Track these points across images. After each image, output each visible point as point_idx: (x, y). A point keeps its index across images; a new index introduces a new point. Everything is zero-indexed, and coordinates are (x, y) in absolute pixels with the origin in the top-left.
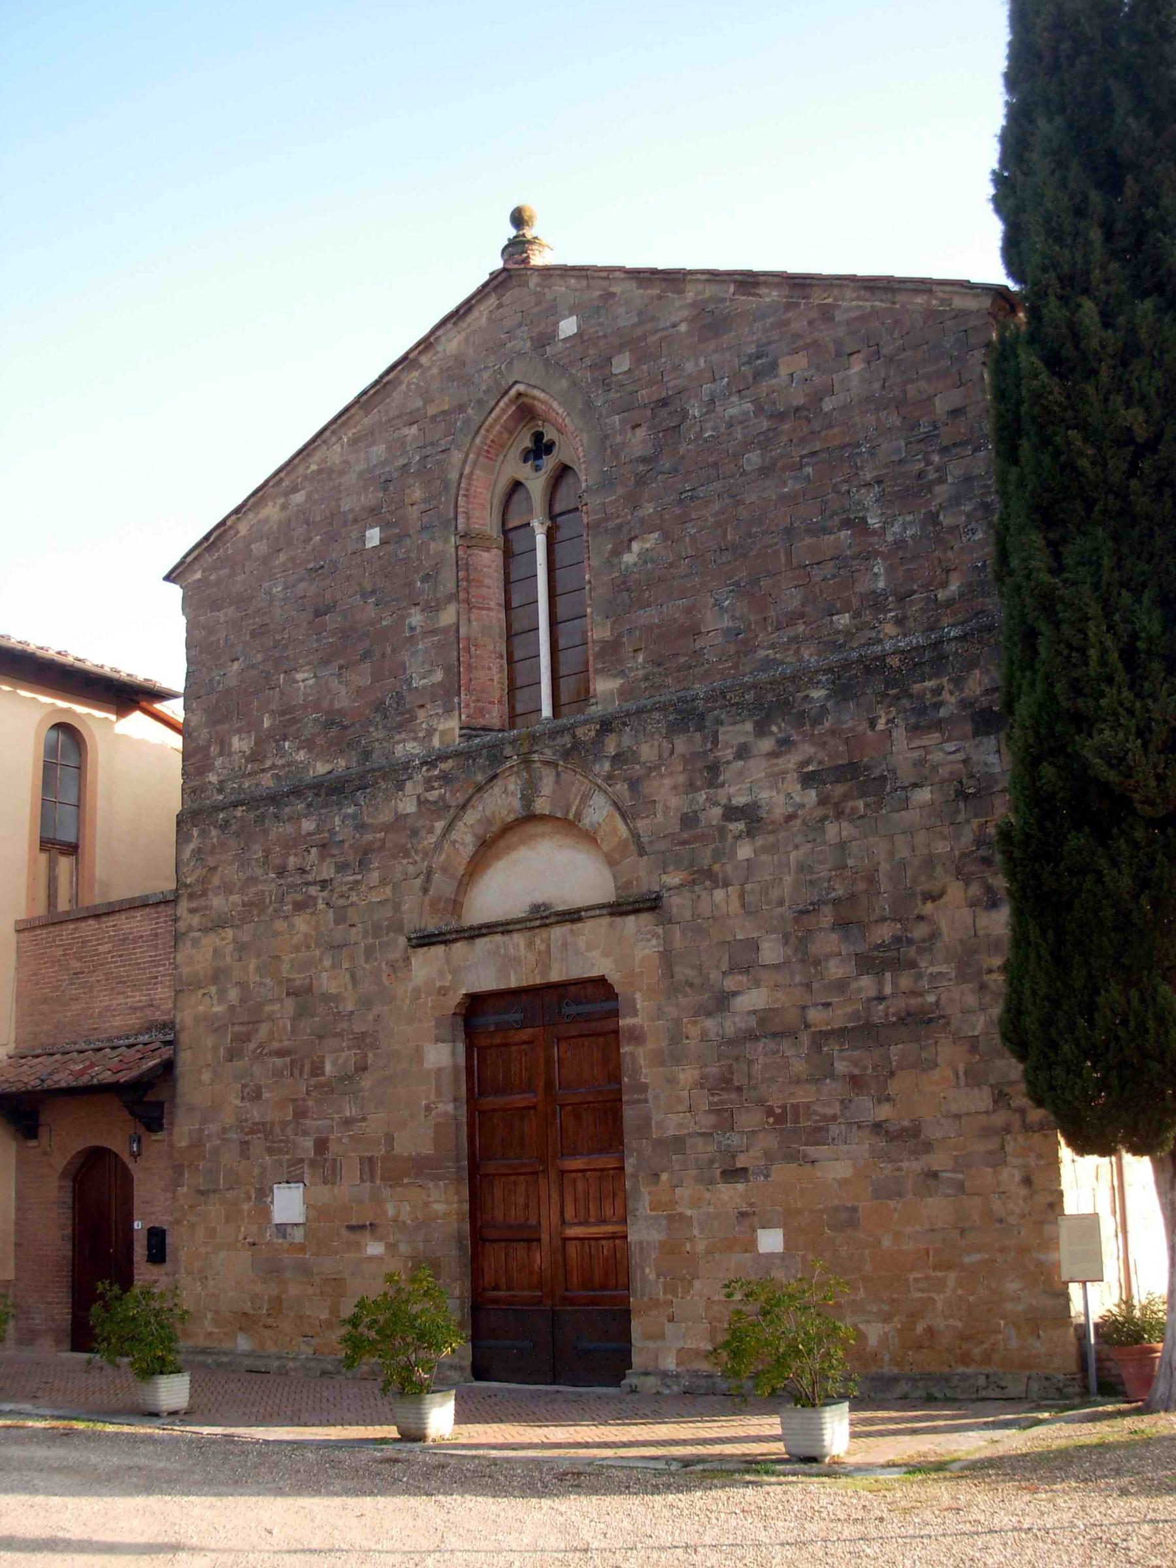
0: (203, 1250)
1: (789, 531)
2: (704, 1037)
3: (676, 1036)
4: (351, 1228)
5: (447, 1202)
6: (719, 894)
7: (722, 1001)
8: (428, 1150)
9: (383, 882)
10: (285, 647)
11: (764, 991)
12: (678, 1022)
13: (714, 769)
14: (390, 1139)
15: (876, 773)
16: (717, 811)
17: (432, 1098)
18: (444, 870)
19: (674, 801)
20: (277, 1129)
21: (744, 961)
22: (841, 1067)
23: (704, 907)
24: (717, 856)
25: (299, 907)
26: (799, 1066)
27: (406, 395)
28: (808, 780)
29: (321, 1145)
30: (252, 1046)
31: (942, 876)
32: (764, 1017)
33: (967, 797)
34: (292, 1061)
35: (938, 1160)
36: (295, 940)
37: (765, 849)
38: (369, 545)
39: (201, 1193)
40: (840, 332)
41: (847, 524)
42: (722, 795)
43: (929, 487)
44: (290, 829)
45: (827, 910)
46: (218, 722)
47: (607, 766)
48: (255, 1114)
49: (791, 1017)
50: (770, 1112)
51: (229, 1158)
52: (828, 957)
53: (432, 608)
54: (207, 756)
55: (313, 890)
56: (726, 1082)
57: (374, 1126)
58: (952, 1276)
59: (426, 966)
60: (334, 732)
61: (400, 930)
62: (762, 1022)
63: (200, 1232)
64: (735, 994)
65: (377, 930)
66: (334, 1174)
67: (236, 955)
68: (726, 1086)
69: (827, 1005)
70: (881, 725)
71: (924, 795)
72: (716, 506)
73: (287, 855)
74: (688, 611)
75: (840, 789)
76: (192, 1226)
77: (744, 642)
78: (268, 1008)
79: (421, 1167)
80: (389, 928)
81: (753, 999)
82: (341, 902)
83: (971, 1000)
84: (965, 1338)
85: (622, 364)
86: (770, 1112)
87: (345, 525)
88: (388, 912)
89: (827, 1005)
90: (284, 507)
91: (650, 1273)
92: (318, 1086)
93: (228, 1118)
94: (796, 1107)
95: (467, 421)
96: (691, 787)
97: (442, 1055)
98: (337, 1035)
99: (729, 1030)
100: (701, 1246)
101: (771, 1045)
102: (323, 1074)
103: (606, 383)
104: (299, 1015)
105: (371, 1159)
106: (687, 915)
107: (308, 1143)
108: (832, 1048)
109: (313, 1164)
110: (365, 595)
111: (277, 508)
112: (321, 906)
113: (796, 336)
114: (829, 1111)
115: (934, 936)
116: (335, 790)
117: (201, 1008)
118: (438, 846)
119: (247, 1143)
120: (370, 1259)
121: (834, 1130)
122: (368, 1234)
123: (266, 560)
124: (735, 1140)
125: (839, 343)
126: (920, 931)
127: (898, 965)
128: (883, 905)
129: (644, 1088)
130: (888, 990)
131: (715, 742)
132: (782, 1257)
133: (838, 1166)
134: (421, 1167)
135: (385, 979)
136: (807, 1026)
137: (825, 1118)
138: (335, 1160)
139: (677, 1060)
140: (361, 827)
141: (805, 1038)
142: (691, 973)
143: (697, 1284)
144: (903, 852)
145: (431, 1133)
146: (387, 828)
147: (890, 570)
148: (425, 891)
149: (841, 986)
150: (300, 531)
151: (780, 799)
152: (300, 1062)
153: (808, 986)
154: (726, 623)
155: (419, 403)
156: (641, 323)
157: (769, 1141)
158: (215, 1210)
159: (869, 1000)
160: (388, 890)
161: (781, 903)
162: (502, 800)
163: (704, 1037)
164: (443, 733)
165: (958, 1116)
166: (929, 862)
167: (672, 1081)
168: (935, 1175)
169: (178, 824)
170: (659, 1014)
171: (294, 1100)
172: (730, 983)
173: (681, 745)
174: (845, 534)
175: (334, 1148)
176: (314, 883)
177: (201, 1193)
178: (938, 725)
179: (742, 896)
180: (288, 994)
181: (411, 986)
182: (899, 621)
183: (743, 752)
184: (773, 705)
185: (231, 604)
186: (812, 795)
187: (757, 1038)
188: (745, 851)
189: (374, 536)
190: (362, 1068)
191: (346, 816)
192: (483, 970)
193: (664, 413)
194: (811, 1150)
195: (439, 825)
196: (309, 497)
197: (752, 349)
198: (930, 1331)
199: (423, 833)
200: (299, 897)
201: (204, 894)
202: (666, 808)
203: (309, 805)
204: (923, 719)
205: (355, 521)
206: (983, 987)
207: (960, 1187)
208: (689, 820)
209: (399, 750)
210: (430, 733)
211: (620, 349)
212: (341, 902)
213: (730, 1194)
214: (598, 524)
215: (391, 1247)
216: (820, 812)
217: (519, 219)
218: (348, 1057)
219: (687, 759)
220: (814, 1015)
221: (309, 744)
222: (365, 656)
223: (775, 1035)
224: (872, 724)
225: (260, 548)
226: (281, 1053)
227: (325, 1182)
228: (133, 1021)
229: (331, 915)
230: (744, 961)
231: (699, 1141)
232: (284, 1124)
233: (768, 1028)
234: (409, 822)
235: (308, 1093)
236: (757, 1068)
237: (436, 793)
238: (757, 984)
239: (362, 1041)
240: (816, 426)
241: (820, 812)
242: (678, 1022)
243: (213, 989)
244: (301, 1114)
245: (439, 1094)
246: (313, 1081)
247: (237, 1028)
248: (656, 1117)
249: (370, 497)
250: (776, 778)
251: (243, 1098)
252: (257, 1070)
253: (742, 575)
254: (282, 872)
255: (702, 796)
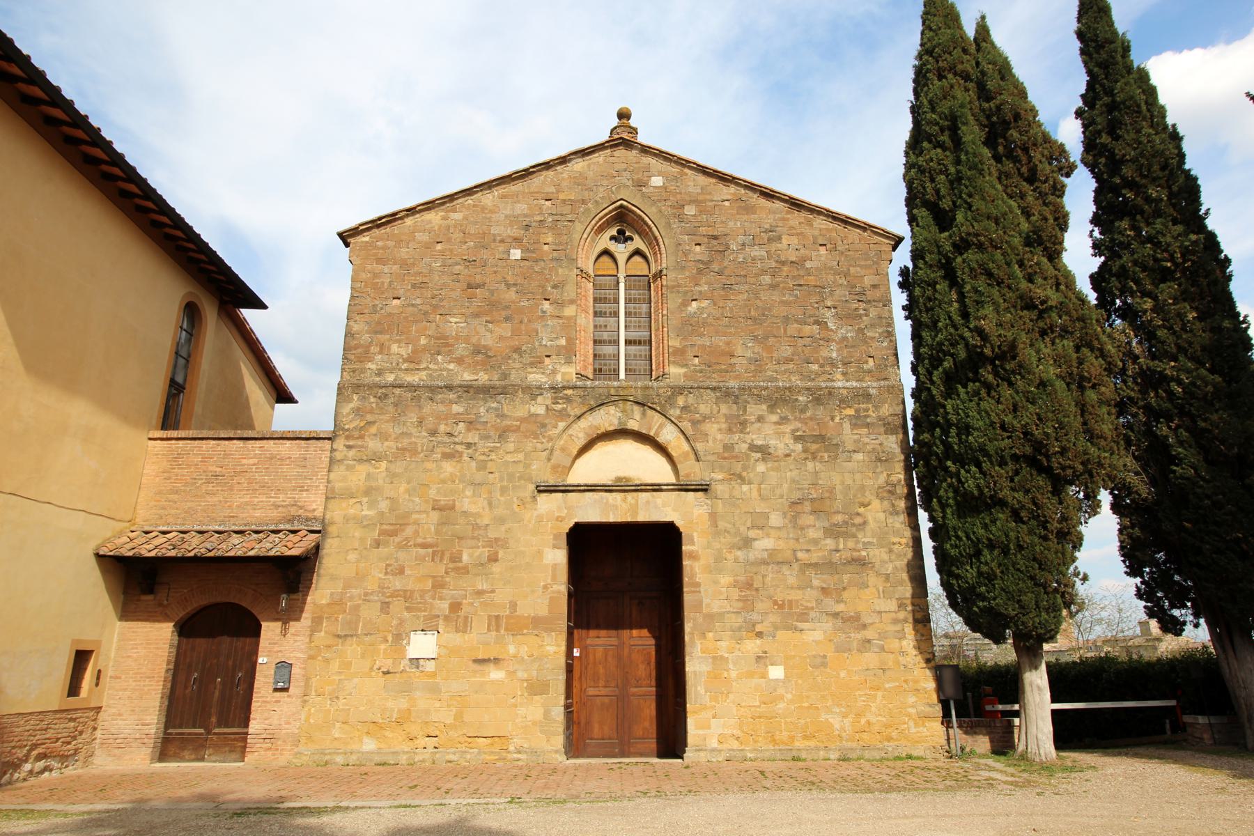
0: (337, 678)
1: (786, 318)
2: (736, 560)
3: (719, 559)
4: (476, 661)
5: (558, 645)
6: (745, 488)
7: (747, 543)
8: (544, 612)
9: (517, 451)
10: (441, 300)
11: (772, 540)
12: (720, 551)
13: (744, 424)
14: (513, 606)
15: (834, 442)
16: (745, 446)
17: (549, 581)
18: (563, 449)
19: (719, 437)
20: (417, 595)
21: (760, 523)
22: (816, 583)
23: (736, 493)
24: (745, 468)
25: (447, 456)
26: (792, 580)
27: (543, 183)
28: (797, 439)
29: (455, 607)
30: (397, 539)
31: (869, 496)
32: (772, 553)
33: (880, 460)
34: (434, 552)
35: (869, 634)
36: (442, 476)
37: (772, 469)
38: (512, 258)
39: (339, 636)
40: (816, 233)
41: (817, 323)
42: (748, 438)
43: (861, 316)
44: (441, 408)
45: (807, 503)
46: (376, 333)
47: (678, 412)
48: (397, 583)
49: (788, 554)
50: (775, 603)
51: (370, 612)
52: (809, 526)
53: (560, 304)
54: (367, 351)
55: (459, 448)
56: (749, 585)
57: (503, 595)
58: (880, 694)
59: (548, 503)
60: (480, 357)
61: (530, 479)
62: (770, 555)
63: (335, 665)
64: (755, 539)
65: (511, 477)
66: (465, 626)
67: (388, 480)
68: (748, 588)
69: (808, 551)
70: (837, 420)
71: (860, 456)
72: (745, 296)
73: (439, 424)
74: (728, 344)
75: (814, 447)
76: (327, 661)
77: (760, 366)
78: (415, 516)
79: (538, 624)
80: (520, 478)
81: (765, 544)
82: (483, 458)
83: (886, 557)
84: (888, 726)
85: (690, 210)
86: (775, 603)
87: (494, 241)
88: (520, 468)
89: (808, 551)
90: (444, 218)
91: (701, 690)
92: (457, 569)
93: (371, 585)
94: (790, 601)
95: (588, 210)
96: (730, 430)
97: (558, 557)
98: (473, 538)
99: (752, 557)
100: (734, 674)
101: (776, 568)
102: (461, 561)
103: (680, 218)
104: (441, 523)
105: (497, 617)
106: (727, 496)
107: (444, 606)
108: (811, 573)
109: (446, 618)
110: (508, 286)
111: (439, 217)
112: (465, 458)
113: (792, 228)
114: (809, 605)
115: (865, 523)
116: (486, 391)
117: (352, 511)
118: (560, 436)
119: (388, 603)
120: (493, 682)
121: (812, 614)
122: (492, 665)
123: (427, 246)
124: (755, 617)
125: (815, 238)
126: (858, 520)
127: (846, 535)
128: (838, 505)
129: (698, 585)
130: (841, 547)
131: (745, 410)
132: (784, 681)
133: (816, 634)
134: (538, 624)
135: (515, 506)
136: (797, 560)
137: (807, 608)
138: (466, 618)
139: (720, 571)
140: (503, 416)
141: (796, 566)
142: (729, 526)
143: (731, 696)
144: (849, 482)
145: (547, 602)
146: (522, 420)
147: (838, 350)
148: (549, 460)
149: (815, 542)
150: (457, 236)
151: (781, 446)
152: (442, 551)
153: (797, 540)
154: (749, 354)
155: (553, 189)
156: (702, 193)
157: (773, 618)
158: (352, 649)
159: (832, 551)
160: (521, 457)
161: (782, 497)
162: (608, 418)
163: (736, 560)
164: (564, 374)
165: (880, 612)
166: (862, 488)
167: (716, 582)
168: (869, 641)
169: (339, 389)
170: (709, 546)
171: (434, 577)
172: (752, 534)
173: (724, 409)
174: (815, 327)
175: (465, 609)
176: (462, 443)
177: (339, 636)
178: (867, 425)
179: (759, 490)
180: (434, 509)
181: (535, 513)
182: (844, 374)
183: (760, 419)
184: (779, 399)
185: (395, 264)
186: (799, 447)
187: (768, 564)
188: (761, 467)
189: (516, 254)
190: (493, 559)
191: (490, 408)
192: (594, 510)
193: (714, 242)
194: (800, 625)
195: (562, 425)
196: (465, 218)
197: (767, 226)
198: (869, 723)
199: (549, 427)
200: (447, 450)
201: (361, 437)
202: (715, 439)
203: (460, 397)
204: (858, 421)
205: (502, 241)
206: (891, 551)
207: (882, 649)
208: (728, 447)
209: (531, 377)
210: (554, 372)
211: (690, 203)
212: (483, 458)
213: (753, 646)
214: (673, 287)
215: (512, 674)
216: (804, 456)
217: (624, 115)
218: (483, 552)
219: (727, 417)
220: (800, 555)
221: (460, 361)
222: (507, 319)
223: (778, 563)
224: (832, 419)
225: (423, 237)
226: (424, 546)
227: (457, 631)
228: (275, 514)
229: (474, 464)
230: (760, 523)
231: (733, 616)
232: (423, 593)
233: (773, 559)
234: (539, 419)
235: (446, 573)
236: (768, 579)
237: (560, 406)
238: (768, 536)
239: (494, 542)
240: (802, 273)
241: (804, 456)
242: (720, 551)
243: (365, 500)
244: (439, 585)
245: (554, 578)
246: (451, 565)
247: (384, 527)
248: (705, 601)
249: (515, 232)
250: (780, 435)
251: (386, 573)
252: (402, 555)
253: (760, 332)
254: (433, 433)
255: (736, 437)
